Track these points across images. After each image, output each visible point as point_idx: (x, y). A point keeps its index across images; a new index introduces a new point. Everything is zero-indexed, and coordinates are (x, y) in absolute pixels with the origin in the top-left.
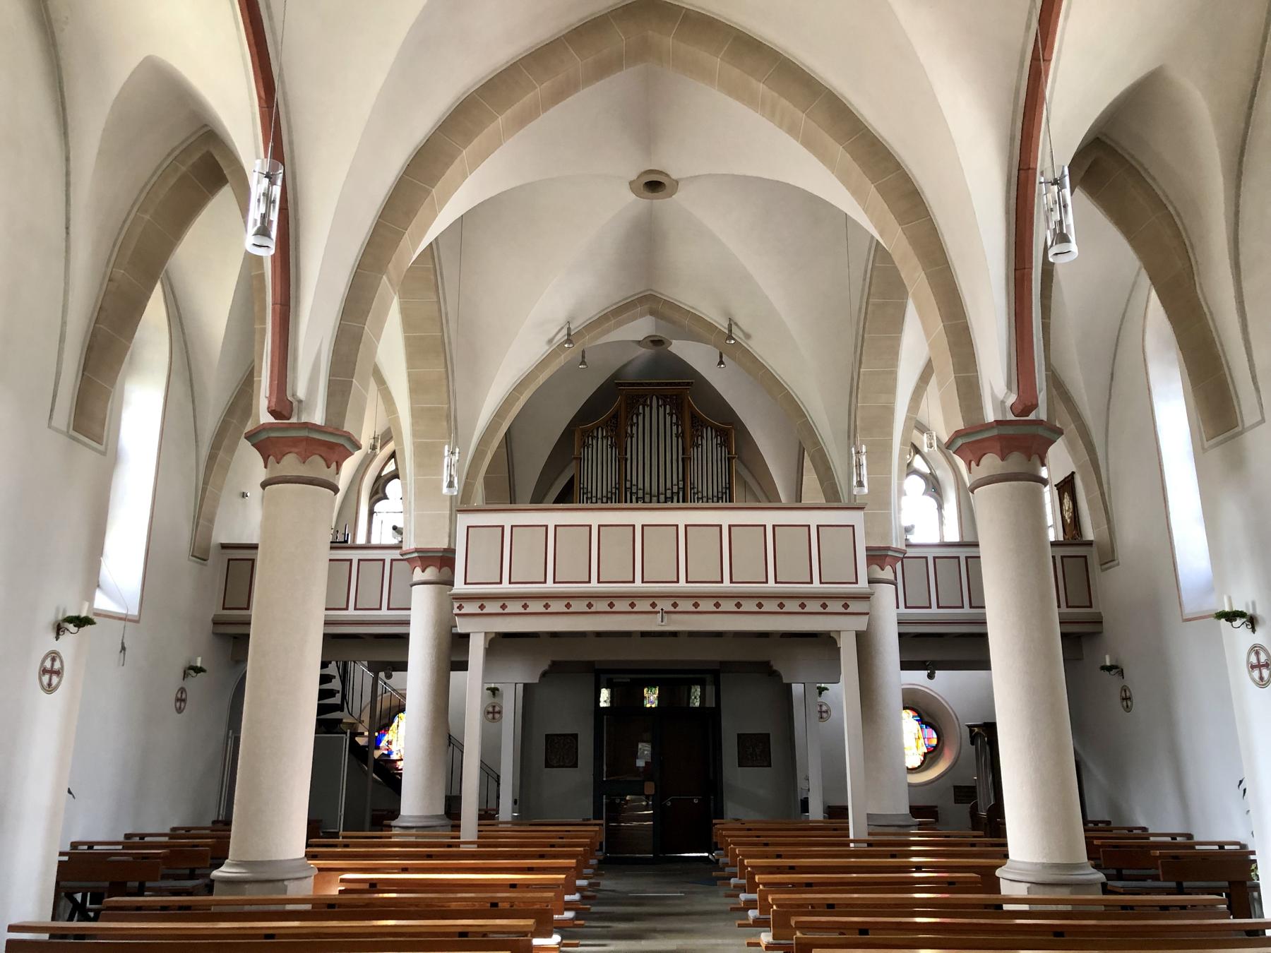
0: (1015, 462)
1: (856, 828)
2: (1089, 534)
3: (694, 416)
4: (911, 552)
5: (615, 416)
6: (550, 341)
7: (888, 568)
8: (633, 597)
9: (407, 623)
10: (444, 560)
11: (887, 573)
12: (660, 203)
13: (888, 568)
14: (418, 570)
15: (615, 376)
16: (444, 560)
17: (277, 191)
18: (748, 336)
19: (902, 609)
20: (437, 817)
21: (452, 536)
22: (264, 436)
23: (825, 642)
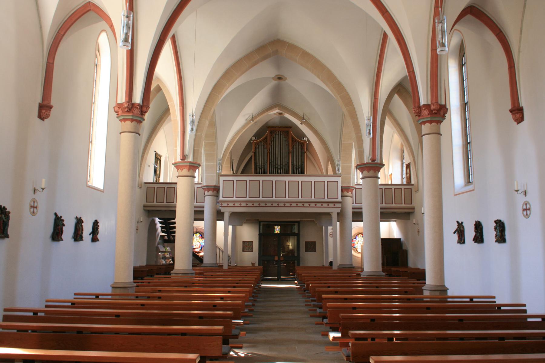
0: (371, 173)
1: (335, 267)
2: (413, 182)
3: (293, 138)
4: (357, 187)
5: (266, 138)
6: (246, 120)
7: (350, 192)
8: (272, 202)
9: (204, 207)
10: (216, 189)
11: (350, 194)
12: (282, 82)
13: (350, 192)
14: (206, 192)
15: (267, 122)
16: (216, 189)
17: (131, 22)
18: (309, 119)
19: (354, 204)
20: (130, 282)
21: (218, 183)
22: (178, 164)
23: (329, 214)
